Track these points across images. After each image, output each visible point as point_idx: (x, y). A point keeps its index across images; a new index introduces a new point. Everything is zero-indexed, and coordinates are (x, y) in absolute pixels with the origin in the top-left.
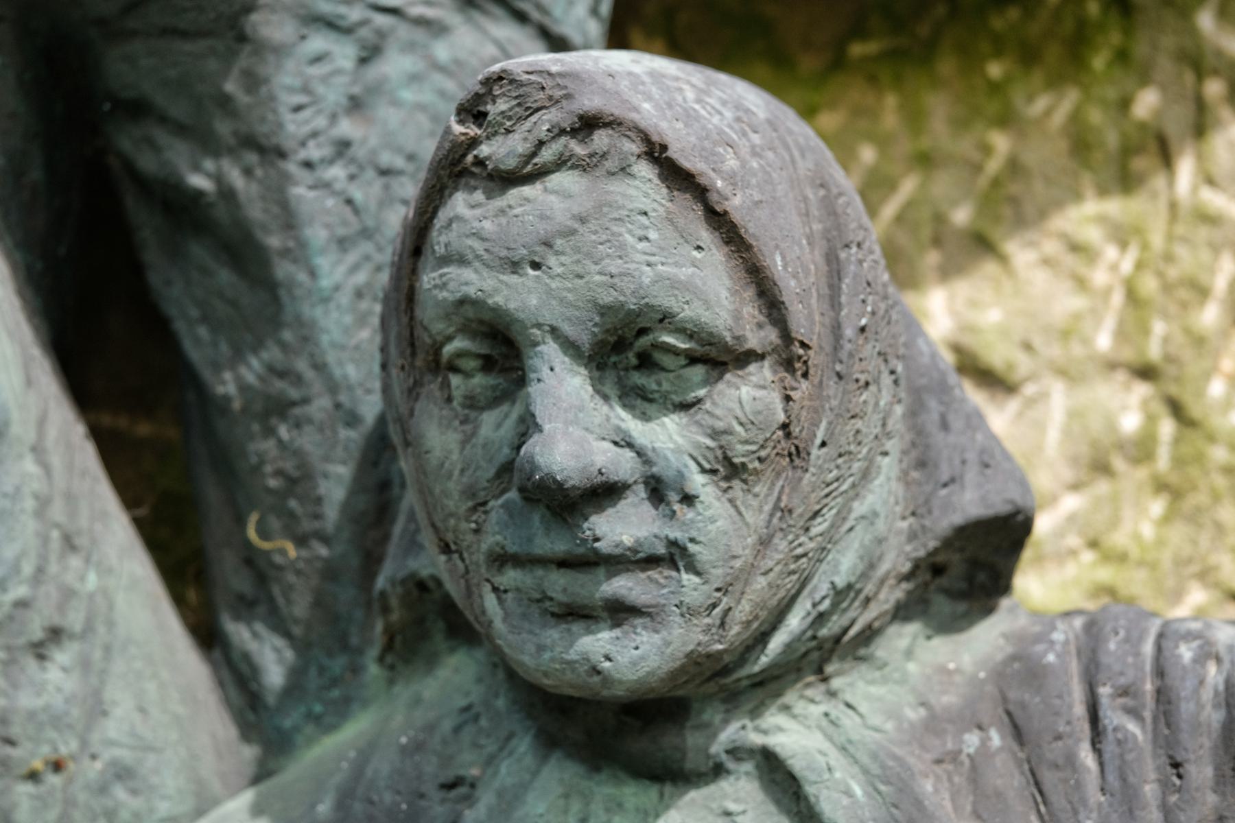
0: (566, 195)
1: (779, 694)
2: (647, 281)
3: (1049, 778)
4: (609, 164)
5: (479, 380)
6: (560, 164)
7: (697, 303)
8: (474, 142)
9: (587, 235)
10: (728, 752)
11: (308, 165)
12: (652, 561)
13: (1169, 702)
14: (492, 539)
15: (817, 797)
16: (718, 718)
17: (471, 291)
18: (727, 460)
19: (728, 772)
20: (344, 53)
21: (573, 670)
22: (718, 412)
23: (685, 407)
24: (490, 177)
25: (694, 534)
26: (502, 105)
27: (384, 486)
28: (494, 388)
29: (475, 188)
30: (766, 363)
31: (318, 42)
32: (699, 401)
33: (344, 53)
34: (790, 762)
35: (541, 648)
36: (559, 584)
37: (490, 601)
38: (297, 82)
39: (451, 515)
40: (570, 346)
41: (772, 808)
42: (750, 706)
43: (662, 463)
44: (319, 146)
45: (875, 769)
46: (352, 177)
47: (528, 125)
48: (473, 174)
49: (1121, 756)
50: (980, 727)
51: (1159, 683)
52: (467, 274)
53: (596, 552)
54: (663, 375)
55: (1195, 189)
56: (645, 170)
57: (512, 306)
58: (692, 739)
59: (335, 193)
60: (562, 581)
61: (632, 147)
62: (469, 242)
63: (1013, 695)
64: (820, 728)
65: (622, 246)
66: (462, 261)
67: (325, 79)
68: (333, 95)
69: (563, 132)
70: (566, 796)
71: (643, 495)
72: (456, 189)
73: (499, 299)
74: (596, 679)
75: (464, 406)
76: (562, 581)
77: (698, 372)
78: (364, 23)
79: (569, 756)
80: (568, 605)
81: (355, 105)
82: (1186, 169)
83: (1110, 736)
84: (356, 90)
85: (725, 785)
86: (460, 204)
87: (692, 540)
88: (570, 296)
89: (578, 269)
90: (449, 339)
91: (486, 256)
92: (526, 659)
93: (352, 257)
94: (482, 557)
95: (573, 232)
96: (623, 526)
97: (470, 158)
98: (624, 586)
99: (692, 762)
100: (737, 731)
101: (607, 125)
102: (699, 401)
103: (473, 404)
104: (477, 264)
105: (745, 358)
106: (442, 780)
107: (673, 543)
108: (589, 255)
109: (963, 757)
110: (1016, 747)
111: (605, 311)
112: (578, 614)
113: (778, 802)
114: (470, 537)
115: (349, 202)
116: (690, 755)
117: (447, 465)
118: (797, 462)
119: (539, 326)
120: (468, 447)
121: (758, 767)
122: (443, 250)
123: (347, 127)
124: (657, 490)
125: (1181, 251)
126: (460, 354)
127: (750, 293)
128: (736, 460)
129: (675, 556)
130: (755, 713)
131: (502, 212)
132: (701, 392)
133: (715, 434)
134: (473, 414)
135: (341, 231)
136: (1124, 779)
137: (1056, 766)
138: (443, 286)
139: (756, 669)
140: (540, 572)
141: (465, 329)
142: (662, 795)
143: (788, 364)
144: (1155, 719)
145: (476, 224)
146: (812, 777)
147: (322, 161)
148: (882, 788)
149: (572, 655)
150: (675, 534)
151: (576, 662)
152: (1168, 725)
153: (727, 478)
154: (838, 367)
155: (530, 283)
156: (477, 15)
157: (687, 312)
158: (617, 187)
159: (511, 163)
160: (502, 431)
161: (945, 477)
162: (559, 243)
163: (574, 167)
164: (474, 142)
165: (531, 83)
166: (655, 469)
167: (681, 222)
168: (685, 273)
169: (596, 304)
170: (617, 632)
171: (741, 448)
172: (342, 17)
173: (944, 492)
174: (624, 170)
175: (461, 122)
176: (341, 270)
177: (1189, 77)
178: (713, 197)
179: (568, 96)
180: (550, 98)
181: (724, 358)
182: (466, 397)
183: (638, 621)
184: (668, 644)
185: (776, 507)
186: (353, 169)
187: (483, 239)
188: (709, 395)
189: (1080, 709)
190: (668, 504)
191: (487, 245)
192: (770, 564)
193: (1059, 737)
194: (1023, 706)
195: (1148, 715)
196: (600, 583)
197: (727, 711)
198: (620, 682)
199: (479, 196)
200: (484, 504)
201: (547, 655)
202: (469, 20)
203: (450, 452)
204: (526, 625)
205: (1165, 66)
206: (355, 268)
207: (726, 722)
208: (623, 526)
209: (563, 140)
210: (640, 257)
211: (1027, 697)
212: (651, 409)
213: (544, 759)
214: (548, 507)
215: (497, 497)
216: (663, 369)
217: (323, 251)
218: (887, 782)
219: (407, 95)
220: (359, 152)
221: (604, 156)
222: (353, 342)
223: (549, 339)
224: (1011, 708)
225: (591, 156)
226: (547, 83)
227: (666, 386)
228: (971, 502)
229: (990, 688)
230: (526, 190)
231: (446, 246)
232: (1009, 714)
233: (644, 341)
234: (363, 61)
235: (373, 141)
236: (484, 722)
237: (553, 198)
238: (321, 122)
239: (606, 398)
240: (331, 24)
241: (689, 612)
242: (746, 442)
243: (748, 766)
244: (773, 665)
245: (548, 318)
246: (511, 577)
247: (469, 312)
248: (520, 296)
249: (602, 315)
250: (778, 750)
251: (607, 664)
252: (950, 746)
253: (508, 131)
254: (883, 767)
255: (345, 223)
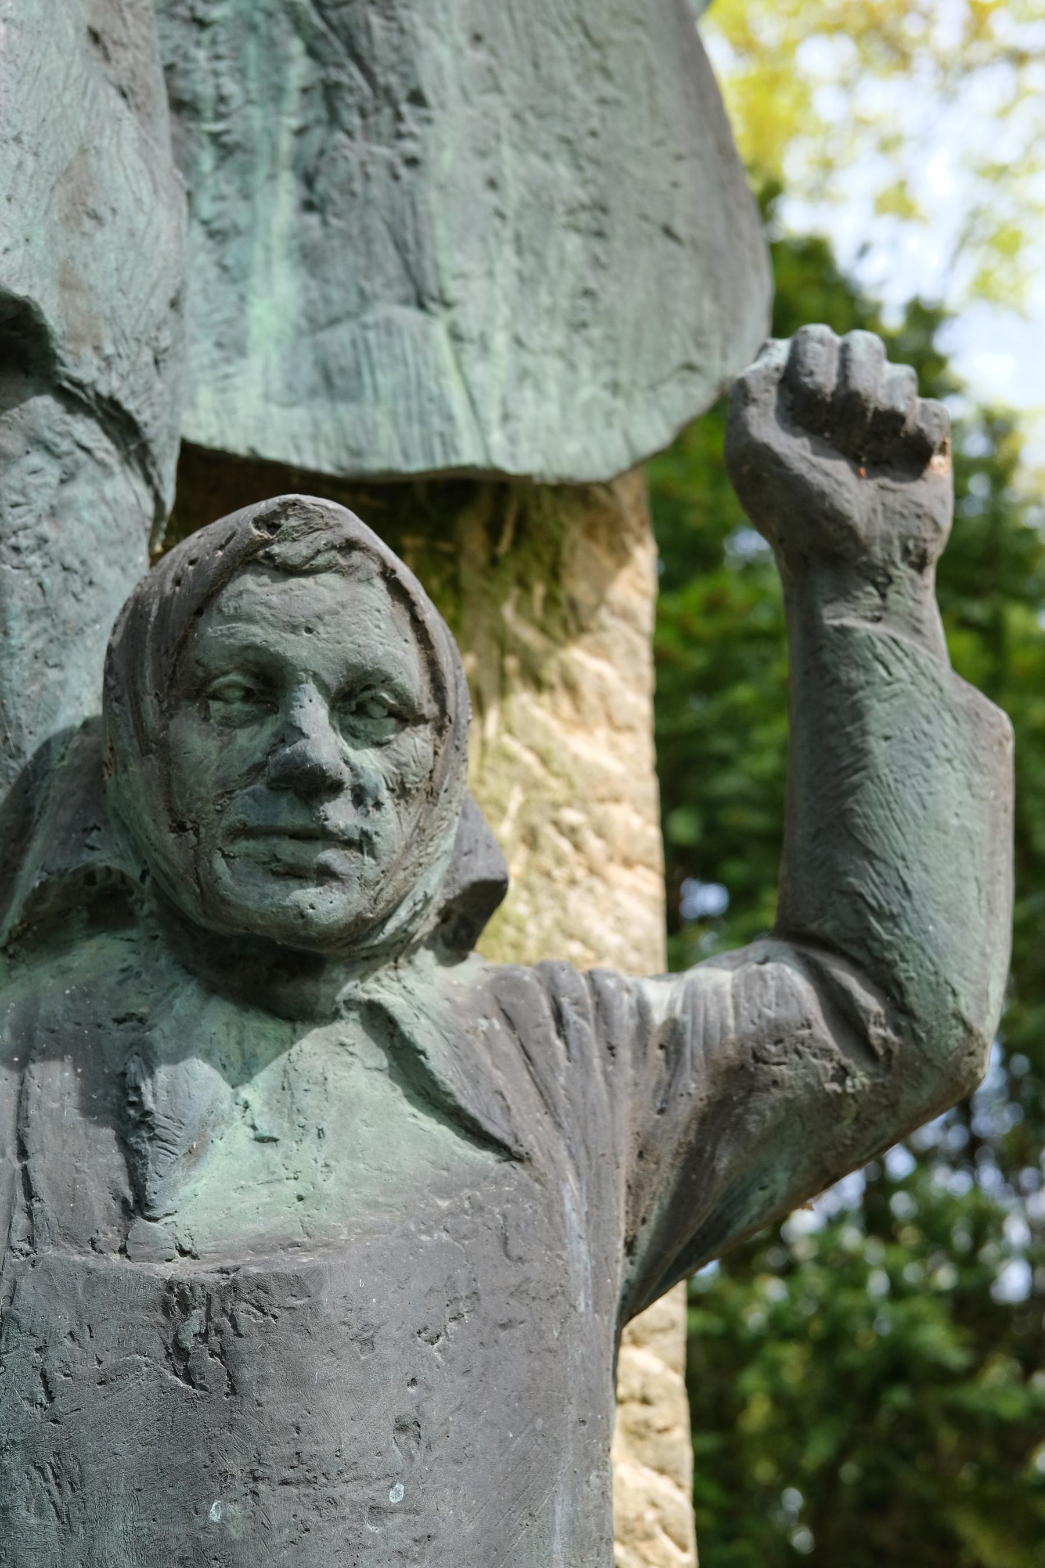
0: (333, 590)
1: (375, 969)
2: (380, 654)
3: (534, 1050)
4: (359, 575)
5: (237, 707)
6: (328, 568)
7: (405, 675)
8: (267, 543)
9: (346, 617)
10: (345, 1002)
11: (16, 549)
12: (349, 844)
13: (606, 1009)
14: (233, 818)
15: (412, 1034)
16: (342, 977)
17: (258, 641)
18: (402, 784)
19: (342, 1017)
20: (53, 472)
21: (285, 914)
22: (402, 751)
23: (379, 745)
24: (276, 568)
25: (378, 829)
26: (293, 522)
27: (29, 810)
28: (248, 713)
29: (262, 574)
30: (429, 726)
31: (37, 459)
32: (389, 742)
33: (53, 472)
34: (390, 1010)
35: (263, 896)
36: (288, 850)
37: (220, 865)
38: (18, 485)
39: (200, 799)
40: (323, 687)
41: (373, 1044)
42: (360, 972)
43: (366, 777)
44: (26, 537)
45: (442, 1023)
46: (45, 567)
47: (310, 538)
48: (261, 564)
49: (580, 1039)
50: (486, 1017)
51: (596, 999)
52: (254, 629)
53: (324, 827)
54: (369, 720)
55: (498, 734)
56: (379, 583)
57: (289, 654)
58: (325, 989)
59: (31, 575)
60: (291, 848)
61: (376, 567)
62: (258, 608)
63: (505, 998)
64: (401, 995)
65: (366, 628)
66: (250, 619)
67: (38, 488)
68: (41, 501)
69: (334, 547)
70: (227, 1024)
71: (350, 798)
72: (244, 572)
73: (279, 649)
74: (300, 921)
75: (220, 724)
76: (291, 848)
77: (392, 722)
78: (69, 453)
79: (226, 999)
80: (291, 866)
81: (53, 513)
82: (493, 717)
83: (572, 1027)
84: (55, 502)
85: (339, 1026)
86: (248, 581)
87: (376, 833)
88: (330, 654)
89: (338, 637)
90: (226, 673)
91: (272, 619)
92: (250, 904)
93: (35, 627)
94: (220, 831)
95: (337, 613)
96: (340, 814)
97: (261, 553)
98: (331, 856)
99: (323, 1006)
100: (353, 988)
101: (361, 549)
102: (389, 742)
103: (227, 722)
104: (263, 623)
105: (421, 720)
106: (115, 1016)
107: (364, 833)
108: (345, 629)
109: (479, 1032)
110: (510, 1031)
111: (351, 667)
112: (298, 874)
113: (376, 1040)
114: (213, 816)
115: (40, 585)
116: (322, 1000)
117: (206, 761)
118: (430, 799)
119: (306, 670)
120: (225, 751)
121: (361, 1016)
122: (232, 611)
123: (46, 528)
124: (360, 796)
125: (489, 778)
126: (230, 686)
127: (427, 677)
128: (408, 786)
129: (362, 843)
130: (363, 978)
131: (285, 592)
132: (392, 737)
133: (399, 765)
134: (227, 730)
135: (31, 605)
136: (582, 1053)
137: (539, 1043)
138: (232, 635)
139: (376, 942)
140: (275, 841)
141: (242, 669)
142: (294, 1031)
143: (440, 730)
144: (596, 1020)
145: (264, 597)
146: (407, 1020)
147: (27, 548)
148: (447, 1035)
149: (287, 903)
150: (367, 827)
151: (288, 907)
152: (606, 1023)
153: (399, 797)
154: (457, 743)
155: (304, 642)
156: (127, 469)
157: (400, 679)
158: (363, 590)
159: (297, 561)
160: (256, 742)
161: (466, 849)
162: (327, 618)
163: (336, 572)
164: (267, 543)
165: (315, 512)
166: (361, 781)
167: (398, 622)
168: (400, 654)
169: (346, 661)
170: (320, 889)
171: (412, 778)
172: (56, 445)
173: (465, 858)
174: (369, 580)
175: (258, 528)
176: (27, 634)
177: (495, 652)
178: (418, 610)
179: (339, 525)
180: (327, 524)
181: (409, 717)
182: (223, 718)
183: (334, 884)
184: (350, 903)
185: (417, 826)
186: (46, 561)
187: (270, 608)
188: (396, 739)
189: (547, 1012)
190: (366, 806)
191: (273, 612)
192: (408, 863)
193: (539, 1025)
194: (513, 1006)
195: (591, 1017)
196: (318, 852)
197: (347, 973)
198: (317, 925)
199: (265, 579)
200: (233, 791)
201: (268, 901)
202: (124, 472)
203: (210, 753)
204: (252, 880)
205: (482, 640)
206: (36, 636)
207: (347, 980)
208: (340, 814)
209: (334, 553)
210: (376, 638)
211: (515, 1000)
212: (357, 742)
213: (206, 1000)
214: (295, 793)
215: (241, 788)
216: (371, 717)
217: (17, 618)
218: (451, 1032)
219: (86, 515)
220: (52, 548)
221: (357, 568)
222: (28, 692)
223: (310, 680)
224: (504, 1007)
225: (350, 567)
226: (326, 513)
227: (370, 729)
228: (480, 870)
229: (488, 995)
230: (303, 581)
231: (236, 609)
232: (503, 1011)
233: (367, 694)
234: (62, 482)
235: (62, 544)
236: (145, 977)
237: (321, 589)
238: (30, 519)
239: (334, 728)
240: (48, 449)
241: (365, 884)
242: (415, 775)
243: (355, 1015)
244: (384, 944)
245: (313, 666)
246: (243, 845)
247: (251, 655)
248: (296, 649)
249: (348, 670)
250: (382, 1001)
251: (311, 911)
252: (471, 1023)
253: (294, 540)
254: (446, 1022)
255: (34, 600)
